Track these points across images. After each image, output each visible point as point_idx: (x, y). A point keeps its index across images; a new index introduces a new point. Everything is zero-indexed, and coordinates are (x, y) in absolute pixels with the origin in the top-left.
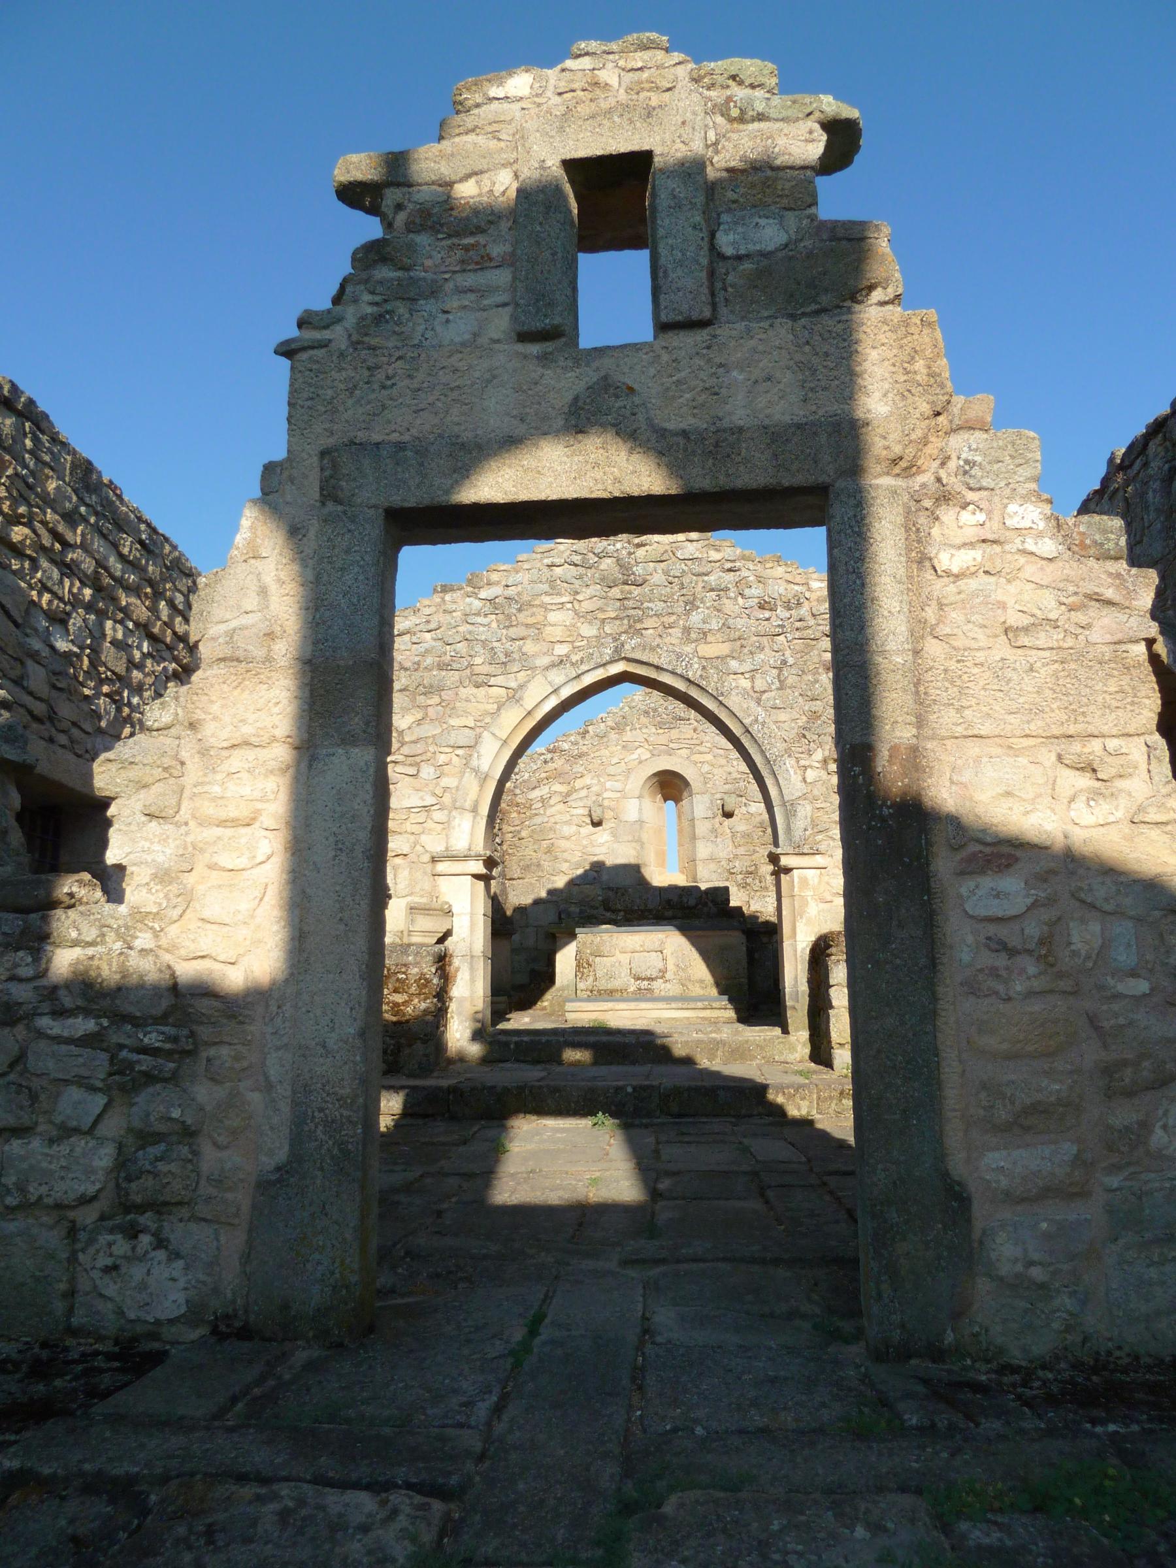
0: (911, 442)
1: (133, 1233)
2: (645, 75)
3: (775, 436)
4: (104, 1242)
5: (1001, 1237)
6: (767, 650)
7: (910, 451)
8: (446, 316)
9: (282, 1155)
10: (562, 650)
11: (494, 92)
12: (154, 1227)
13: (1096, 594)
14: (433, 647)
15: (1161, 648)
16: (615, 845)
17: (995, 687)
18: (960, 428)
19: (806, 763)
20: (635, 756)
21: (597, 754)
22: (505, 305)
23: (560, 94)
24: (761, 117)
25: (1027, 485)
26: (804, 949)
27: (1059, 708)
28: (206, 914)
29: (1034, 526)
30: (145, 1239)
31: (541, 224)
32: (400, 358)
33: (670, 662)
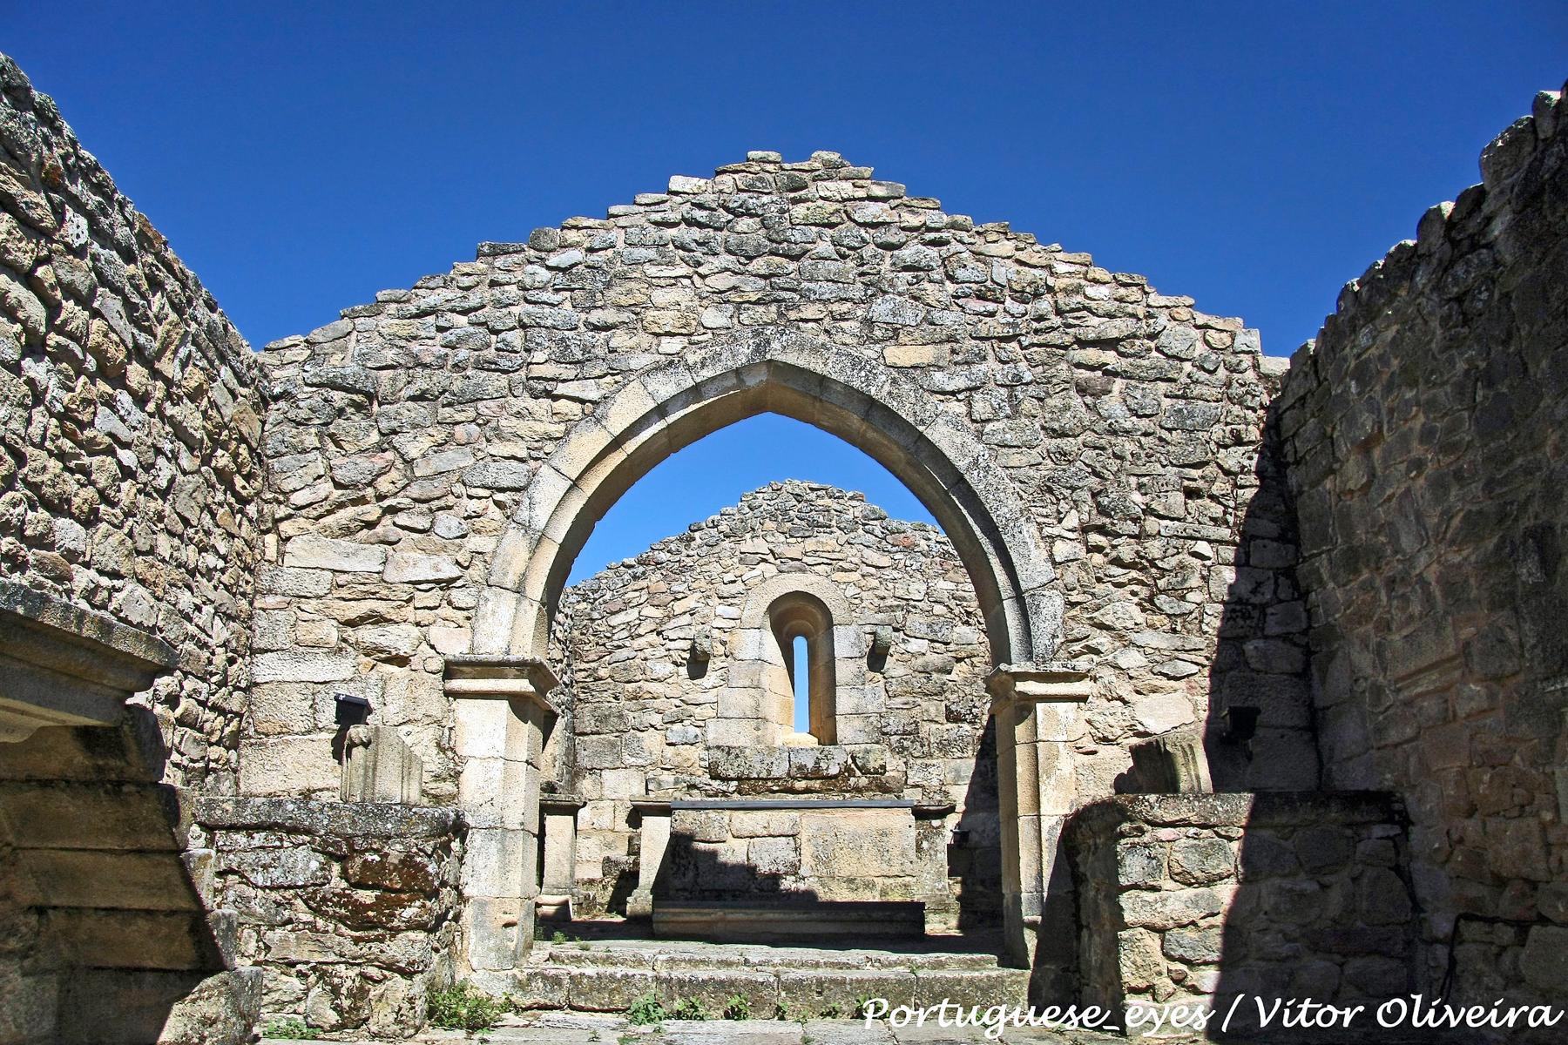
6: (991, 357)
10: (671, 345)
14: (470, 335)
19: (1055, 531)
21: (705, 568)
26: (1052, 828)
33: (842, 370)
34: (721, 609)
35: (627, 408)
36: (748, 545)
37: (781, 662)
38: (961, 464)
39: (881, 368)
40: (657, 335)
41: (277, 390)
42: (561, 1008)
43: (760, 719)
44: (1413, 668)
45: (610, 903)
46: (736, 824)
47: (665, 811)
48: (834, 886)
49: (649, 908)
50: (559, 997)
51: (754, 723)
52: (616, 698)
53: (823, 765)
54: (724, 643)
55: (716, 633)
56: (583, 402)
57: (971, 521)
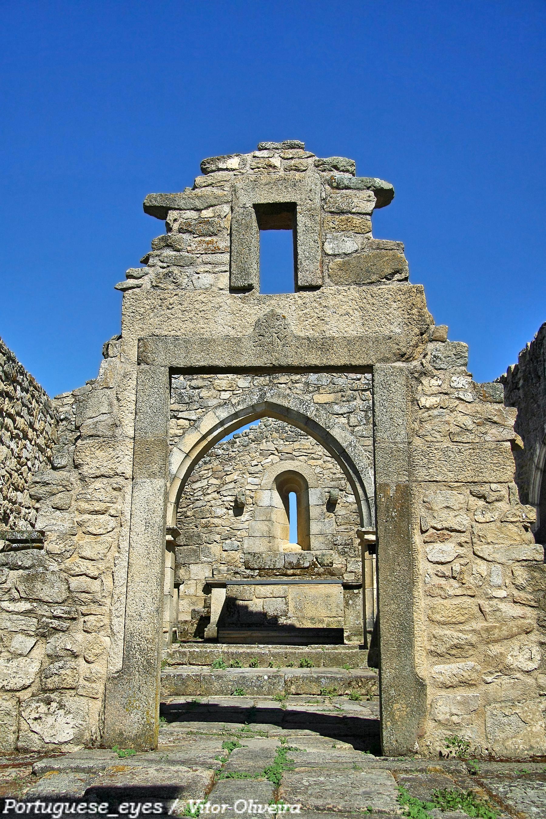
0: (410, 346)
1: (48, 702)
2: (293, 162)
3: (349, 342)
4: (35, 707)
5: (440, 703)
6: (358, 399)
7: (410, 350)
8: (198, 275)
9: (119, 666)
10: (226, 395)
11: (221, 166)
12: (58, 699)
13: (489, 419)
15: (520, 442)
16: (253, 523)
17: (443, 459)
18: (433, 340)
20: (269, 460)
22: (226, 271)
23: (253, 169)
24: (347, 188)
25: (461, 368)
27: (471, 470)
28: (84, 554)
29: (464, 387)
30: (54, 705)
31: (243, 235)
32: (176, 295)
34: (250, 480)
35: (208, 422)
36: (264, 446)
37: (282, 506)
38: (344, 445)
39: (312, 404)
40: (220, 391)
41: (62, 417)
42: (186, 664)
43: (271, 537)
44: (366, 570)
45: (195, 633)
46: (257, 591)
47: (223, 585)
48: (305, 623)
49: (215, 634)
50: (185, 660)
51: (268, 539)
52: (196, 527)
53: (301, 562)
54: (252, 498)
55: (248, 492)
56: (189, 420)
57: (348, 467)
